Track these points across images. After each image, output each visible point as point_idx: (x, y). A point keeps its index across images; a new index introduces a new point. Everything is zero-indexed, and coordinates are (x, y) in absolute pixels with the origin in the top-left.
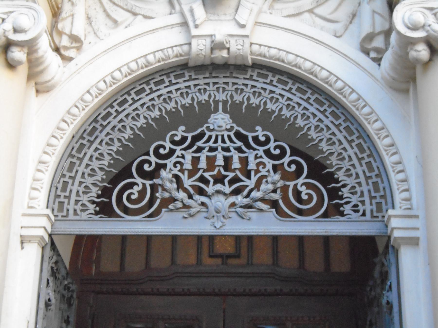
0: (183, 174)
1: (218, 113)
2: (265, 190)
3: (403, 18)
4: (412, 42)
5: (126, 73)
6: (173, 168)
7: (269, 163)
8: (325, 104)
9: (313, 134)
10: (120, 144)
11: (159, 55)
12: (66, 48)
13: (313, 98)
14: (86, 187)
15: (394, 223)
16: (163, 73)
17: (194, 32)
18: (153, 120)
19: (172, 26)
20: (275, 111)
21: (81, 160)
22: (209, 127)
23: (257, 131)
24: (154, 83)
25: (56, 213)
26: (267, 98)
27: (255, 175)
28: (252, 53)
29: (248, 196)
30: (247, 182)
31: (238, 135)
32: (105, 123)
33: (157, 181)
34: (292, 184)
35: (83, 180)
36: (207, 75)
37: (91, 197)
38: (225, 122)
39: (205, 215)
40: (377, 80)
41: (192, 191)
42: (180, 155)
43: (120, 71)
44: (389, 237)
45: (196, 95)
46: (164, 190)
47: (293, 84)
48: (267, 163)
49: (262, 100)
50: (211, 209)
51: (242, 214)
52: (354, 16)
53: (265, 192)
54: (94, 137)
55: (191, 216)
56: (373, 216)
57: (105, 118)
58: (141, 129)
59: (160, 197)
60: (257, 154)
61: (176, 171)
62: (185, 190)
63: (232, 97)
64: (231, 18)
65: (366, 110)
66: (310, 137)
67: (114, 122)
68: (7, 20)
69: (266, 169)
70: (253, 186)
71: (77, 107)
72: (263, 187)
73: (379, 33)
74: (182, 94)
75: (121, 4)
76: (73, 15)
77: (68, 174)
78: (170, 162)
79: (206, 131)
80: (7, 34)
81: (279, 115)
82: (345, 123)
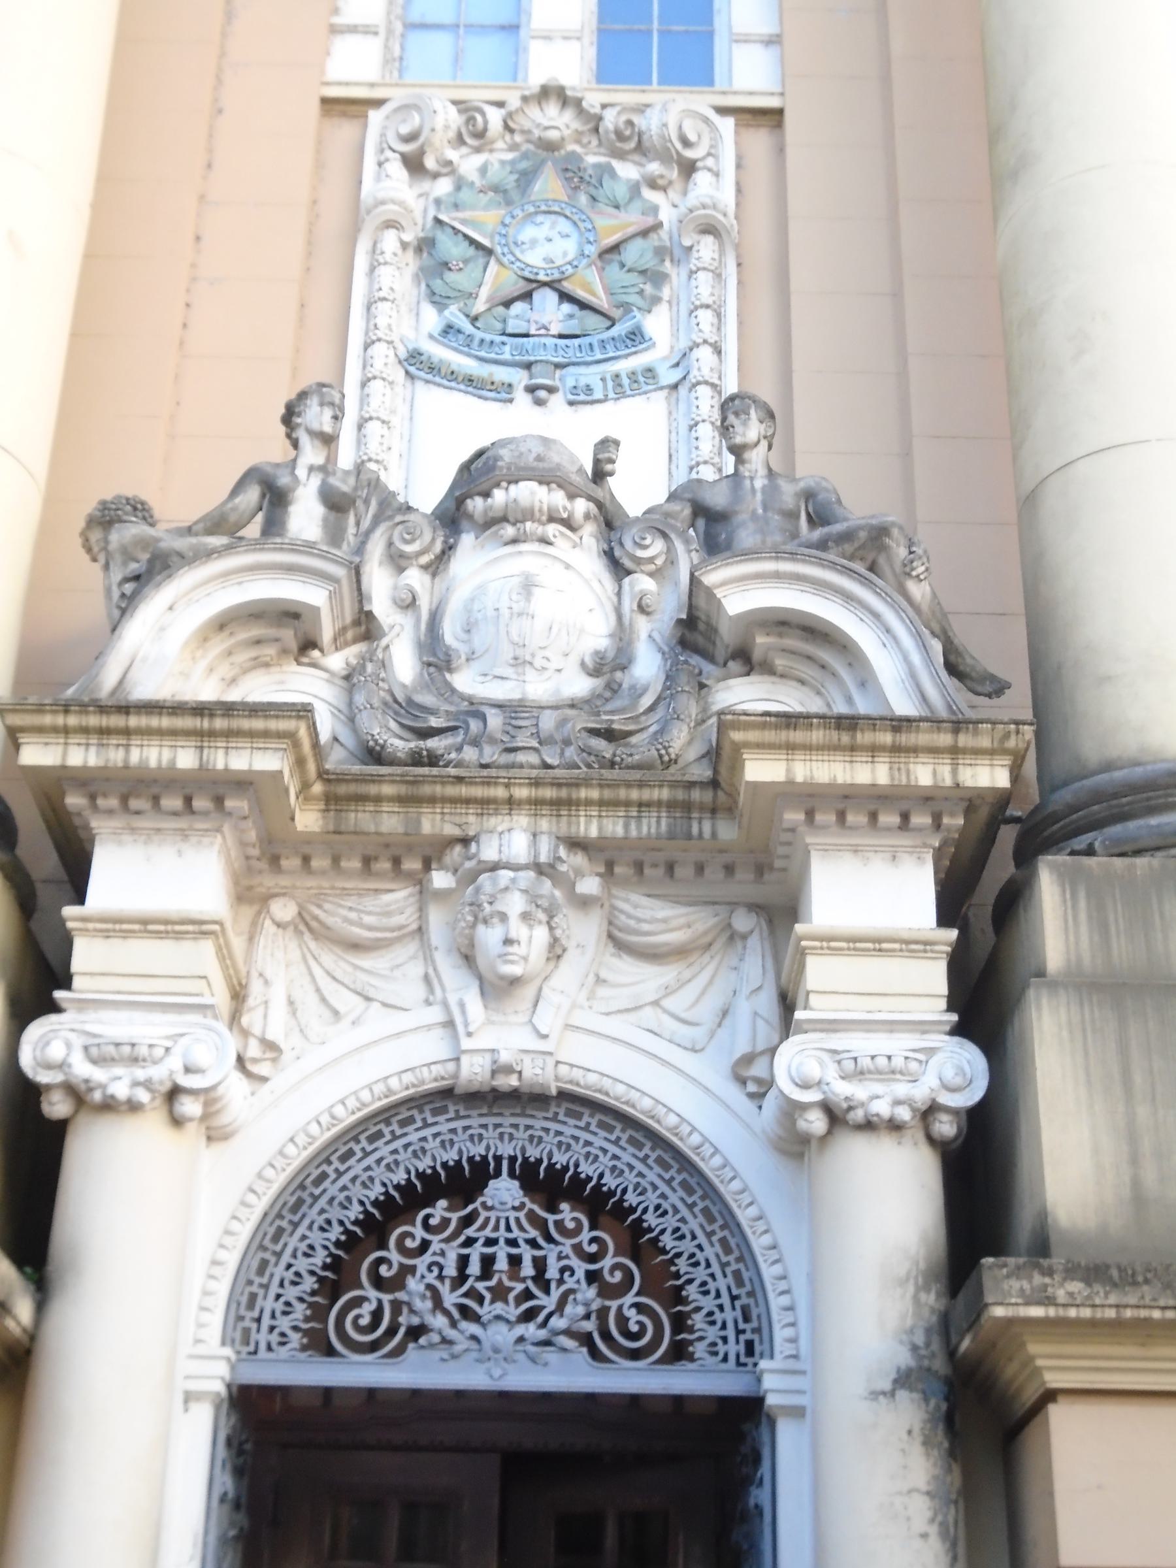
0: (443, 1283)
3: (789, 1067)
4: (803, 1107)
6: (426, 1273)
7: (581, 1267)
10: (341, 1229)
11: (408, 1078)
12: (255, 1061)
13: (654, 1156)
14: (288, 1304)
15: (769, 1382)
16: (413, 1104)
17: (466, 1043)
19: (429, 1027)
21: (278, 1255)
24: (399, 1122)
25: (238, 1347)
27: (558, 1287)
28: (557, 1079)
31: (532, 1217)
32: (317, 1192)
33: (401, 1296)
34: (614, 1305)
36: (485, 1111)
40: (755, 1133)
41: (456, 1314)
43: (344, 1103)
46: (412, 1311)
47: (623, 1131)
50: (486, 1345)
52: (725, 1013)
54: (299, 1215)
55: (454, 1357)
56: (739, 1364)
57: (319, 1181)
58: (376, 1203)
61: (431, 1278)
64: (526, 1019)
65: (736, 1185)
67: (333, 1190)
68: (172, 1051)
69: (575, 1278)
70: (551, 1308)
71: (273, 1166)
72: (569, 1309)
73: (762, 1053)
74: (443, 1142)
75: (346, 982)
76: (266, 1002)
77: (257, 1280)
78: (422, 1263)
79: (480, 1210)
80: (174, 1076)
81: (599, 1185)
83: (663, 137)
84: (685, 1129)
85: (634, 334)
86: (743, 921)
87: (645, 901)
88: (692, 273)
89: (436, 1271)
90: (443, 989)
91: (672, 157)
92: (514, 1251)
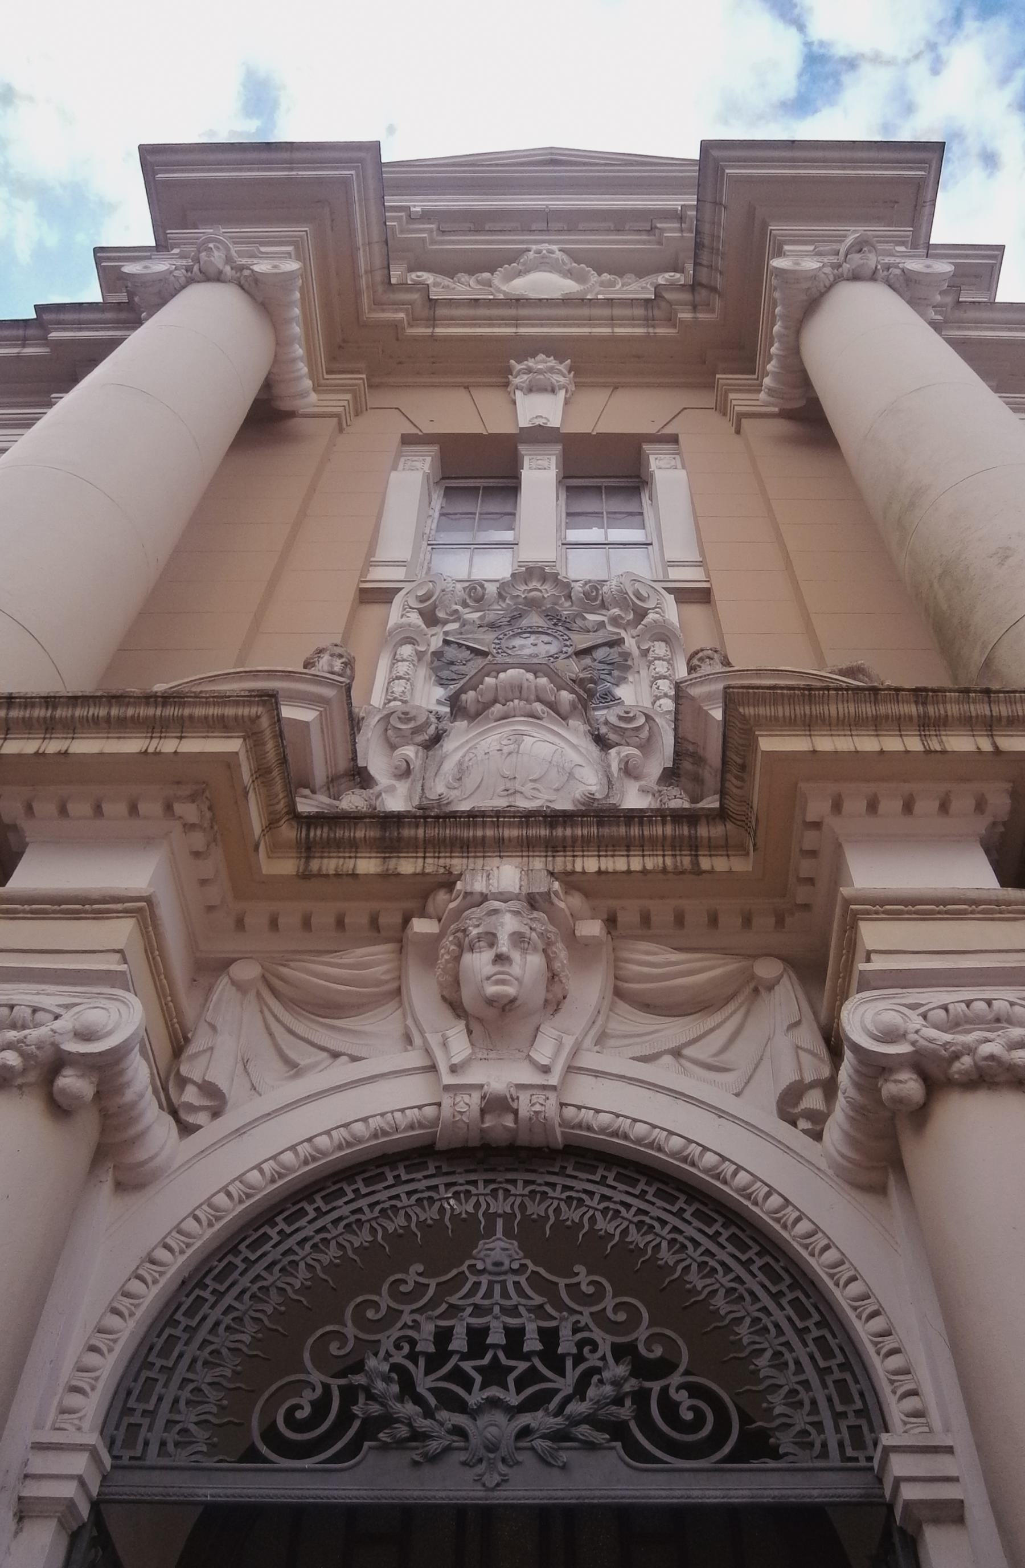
1: (494, 1238)
2: (597, 1398)
3: (862, 1022)
5: (305, 1156)
6: (392, 1350)
8: (716, 1221)
9: (695, 1279)
12: (192, 1108)
15: (900, 1466)
18: (355, 1250)
20: (614, 1235)
22: (475, 1265)
23: (578, 1274)
26: (596, 1209)
29: (560, 1411)
30: (558, 1382)
31: (535, 1280)
34: (656, 1386)
35: (190, 1376)
37: (205, 1413)
38: (510, 1256)
39: (463, 1456)
41: (433, 1402)
42: (410, 1324)
44: (890, 1507)
45: (449, 1204)
46: (371, 1397)
48: (599, 1341)
49: (585, 1213)
50: (475, 1440)
51: (545, 1454)
53: (598, 1401)
55: (433, 1459)
59: (359, 1414)
60: (578, 1322)
61: (398, 1358)
62: (418, 1400)
63: (523, 1207)
65: (803, 1227)
66: (688, 1286)
69: (599, 1354)
70: (570, 1390)
72: (592, 1392)
73: (813, 1085)
78: (387, 1342)
82: (761, 1257)
83: (621, 591)
84: (729, 1169)
85: (606, 695)
86: (767, 969)
87: (652, 947)
88: (651, 662)
89: (407, 1348)
90: (422, 1033)
91: (629, 606)
92: (513, 1322)
